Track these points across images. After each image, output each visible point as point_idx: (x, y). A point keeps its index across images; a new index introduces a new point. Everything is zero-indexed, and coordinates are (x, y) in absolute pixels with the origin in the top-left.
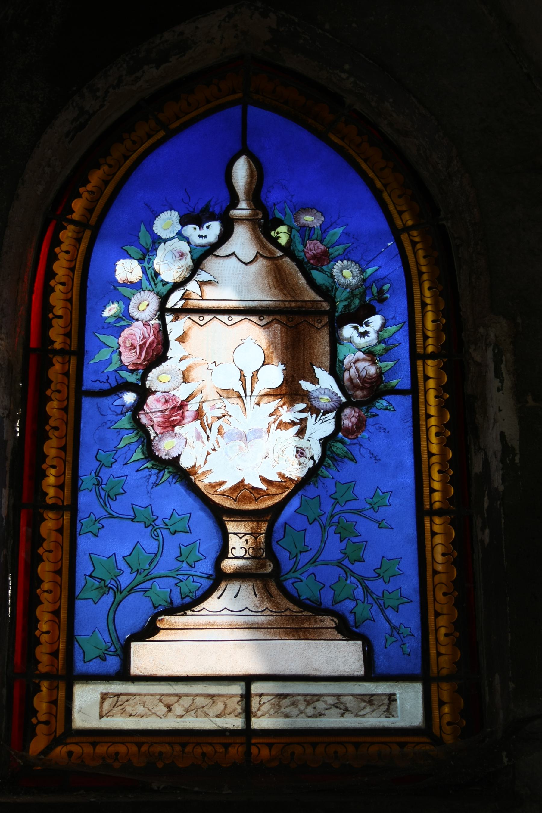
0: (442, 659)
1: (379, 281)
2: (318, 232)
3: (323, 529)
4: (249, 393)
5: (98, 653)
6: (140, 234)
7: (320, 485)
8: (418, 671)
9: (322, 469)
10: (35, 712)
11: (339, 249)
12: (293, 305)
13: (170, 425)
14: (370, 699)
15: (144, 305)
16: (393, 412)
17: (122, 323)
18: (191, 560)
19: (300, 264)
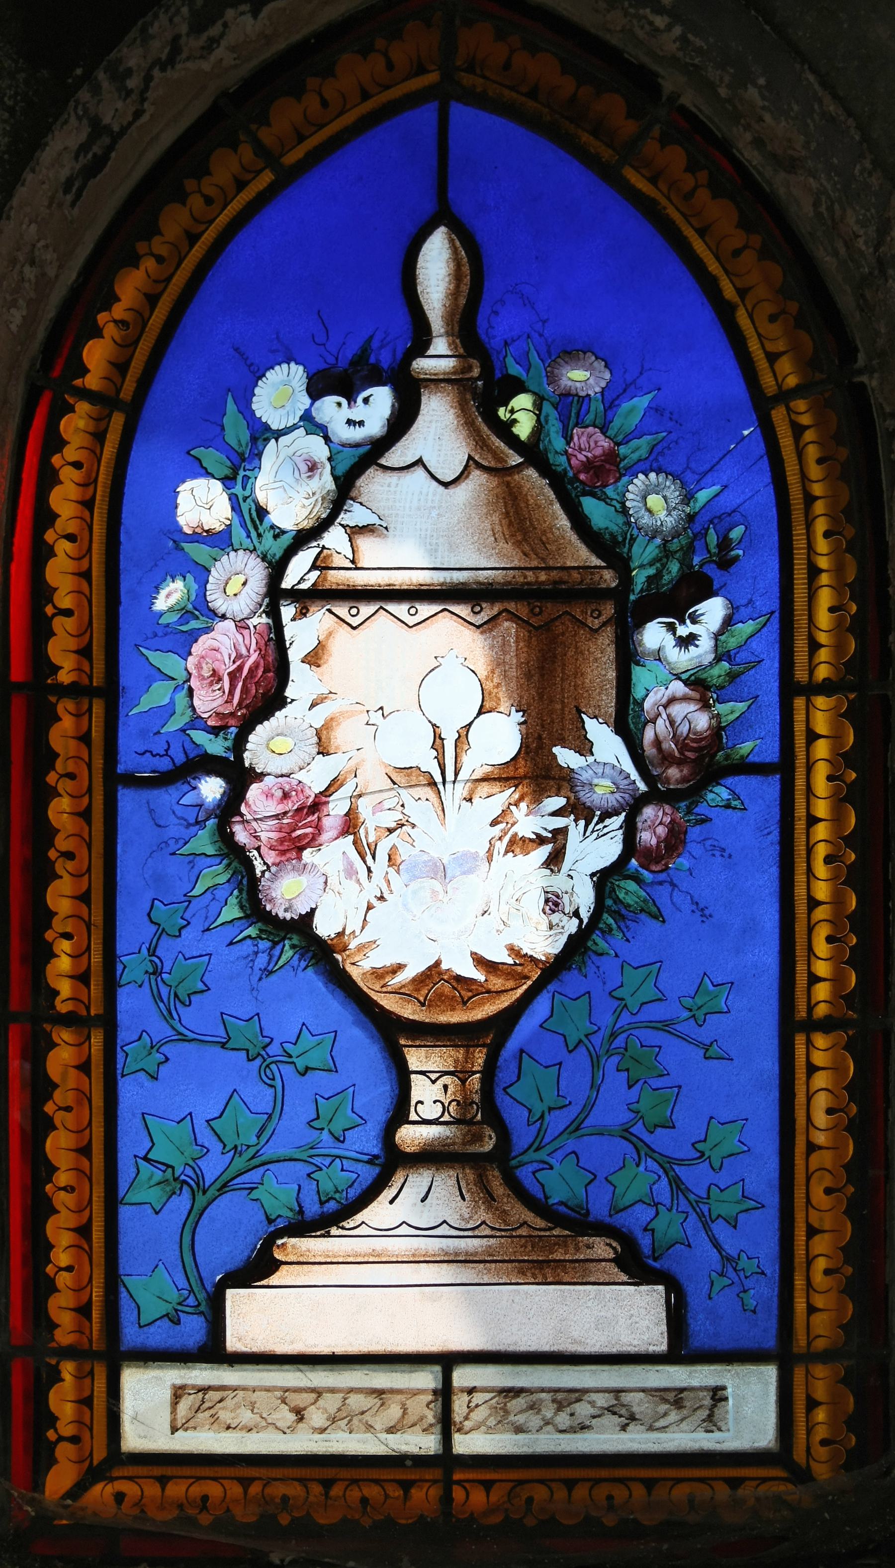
1: (723, 520)
2: (597, 407)
3: (595, 1062)
4: (450, 776)
5: (164, 1308)
7: (590, 969)
8: (770, 1342)
9: (596, 937)
11: (640, 447)
12: (543, 577)
15: (237, 584)
16: (739, 812)
17: (194, 624)
19: (558, 482)
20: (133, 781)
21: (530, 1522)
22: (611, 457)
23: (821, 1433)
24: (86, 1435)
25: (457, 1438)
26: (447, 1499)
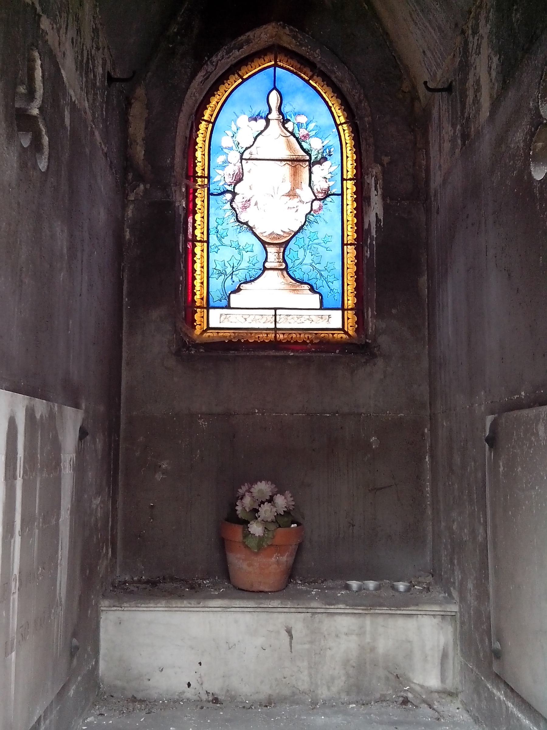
0: (350, 302)
1: (329, 147)
2: (305, 125)
3: (305, 250)
4: (276, 193)
5: (219, 298)
6: (232, 126)
7: (304, 233)
8: (340, 307)
9: (305, 226)
10: (195, 321)
11: (313, 133)
12: (294, 157)
13: (245, 208)
14: (322, 317)
15: (234, 157)
16: (333, 203)
17: (225, 165)
18: (253, 263)
19: (297, 139)
20: (212, 194)
21: (292, 341)
22: (308, 135)
23: (350, 324)
24: (202, 324)
25: (277, 324)
26: (275, 337)
